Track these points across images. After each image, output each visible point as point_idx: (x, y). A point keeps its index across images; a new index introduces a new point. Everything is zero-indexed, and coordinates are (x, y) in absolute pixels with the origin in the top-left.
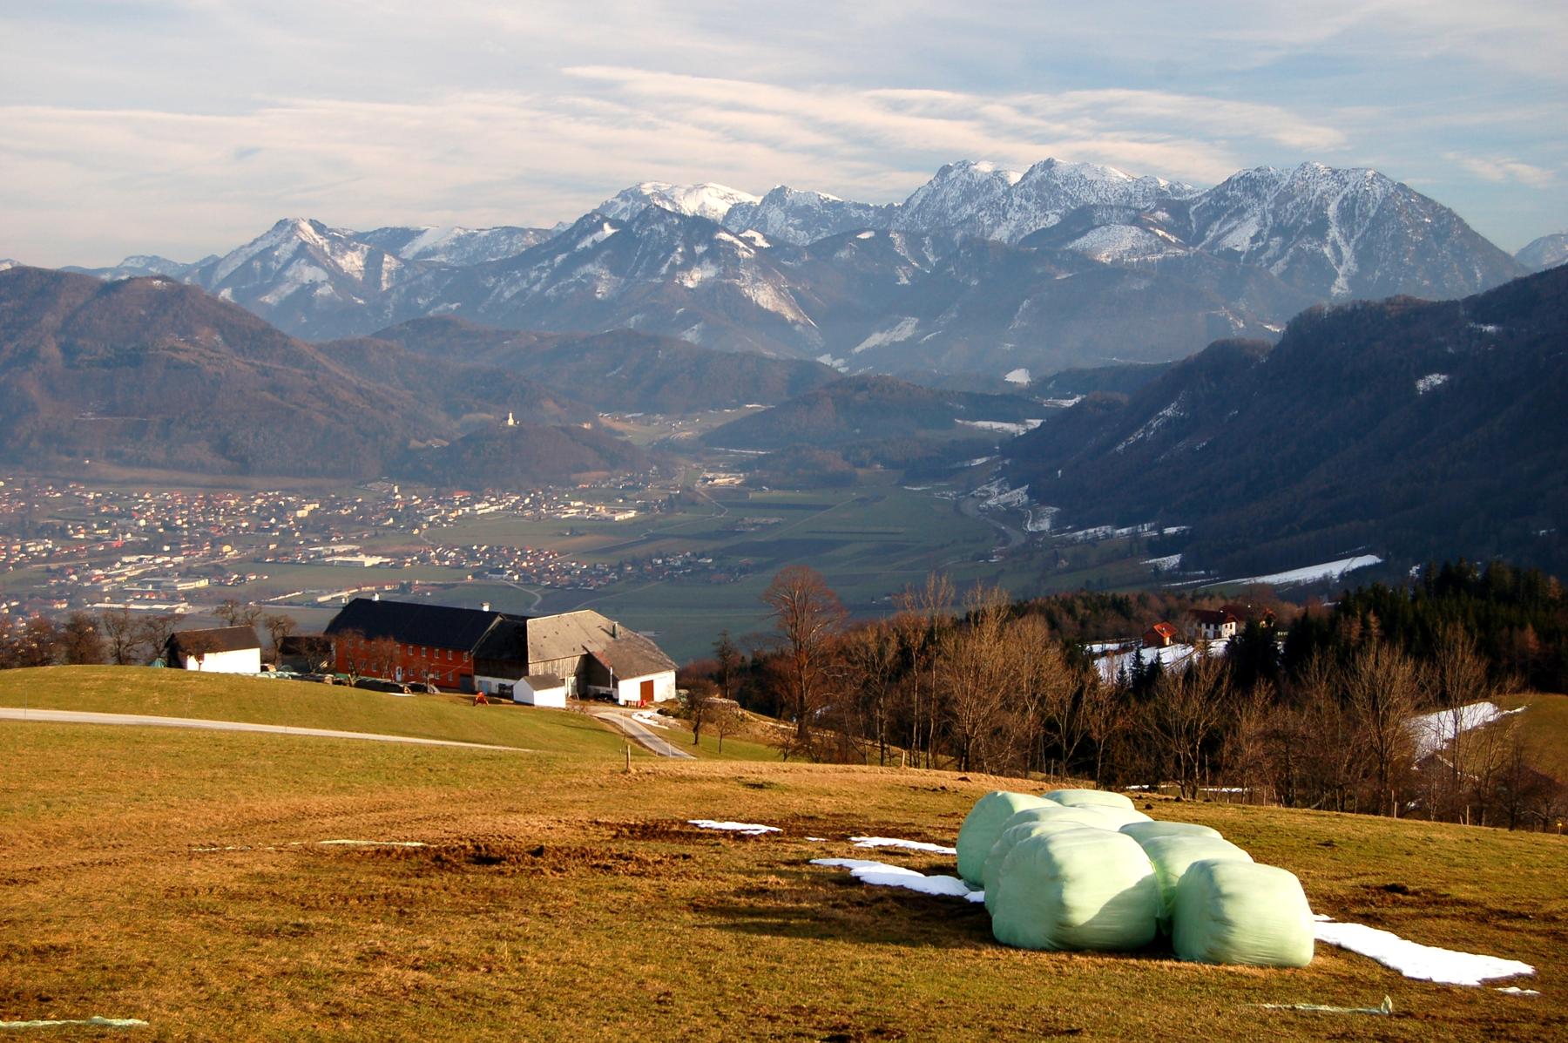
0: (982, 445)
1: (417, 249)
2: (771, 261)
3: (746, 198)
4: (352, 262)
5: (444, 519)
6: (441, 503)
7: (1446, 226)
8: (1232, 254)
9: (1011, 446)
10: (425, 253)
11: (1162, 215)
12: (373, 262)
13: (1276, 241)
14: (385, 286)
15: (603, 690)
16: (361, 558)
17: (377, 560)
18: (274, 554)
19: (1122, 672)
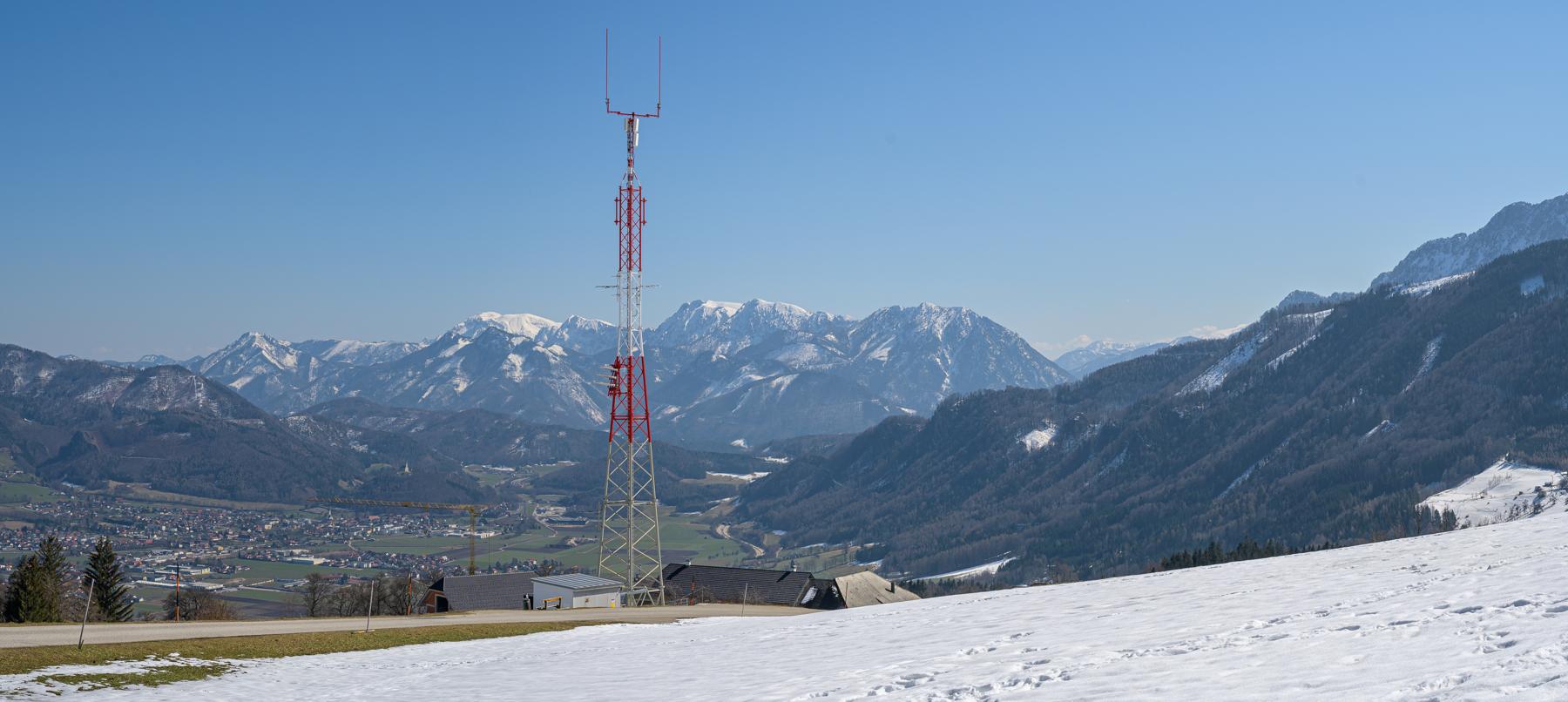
0: (723, 490)
1: (333, 353)
2: (573, 359)
3: (551, 323)
4: (290, 360)
5: (364, 534)
6: (362, 523)
7: (1014, 348)
8: (877, 362)
9: (748, 492)
10: (339, 357)
11: (831, 337)
12: (303, 361)
13: (905, 354)
14: (311, 379)
15: (621, 335)
16: (311, 559)
17: (321, 561)
18: (252, 553)
19: (332, 343)
